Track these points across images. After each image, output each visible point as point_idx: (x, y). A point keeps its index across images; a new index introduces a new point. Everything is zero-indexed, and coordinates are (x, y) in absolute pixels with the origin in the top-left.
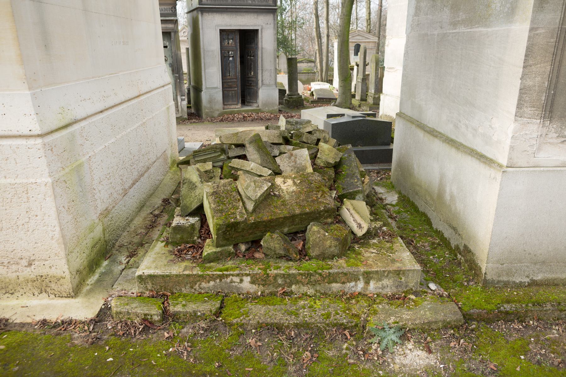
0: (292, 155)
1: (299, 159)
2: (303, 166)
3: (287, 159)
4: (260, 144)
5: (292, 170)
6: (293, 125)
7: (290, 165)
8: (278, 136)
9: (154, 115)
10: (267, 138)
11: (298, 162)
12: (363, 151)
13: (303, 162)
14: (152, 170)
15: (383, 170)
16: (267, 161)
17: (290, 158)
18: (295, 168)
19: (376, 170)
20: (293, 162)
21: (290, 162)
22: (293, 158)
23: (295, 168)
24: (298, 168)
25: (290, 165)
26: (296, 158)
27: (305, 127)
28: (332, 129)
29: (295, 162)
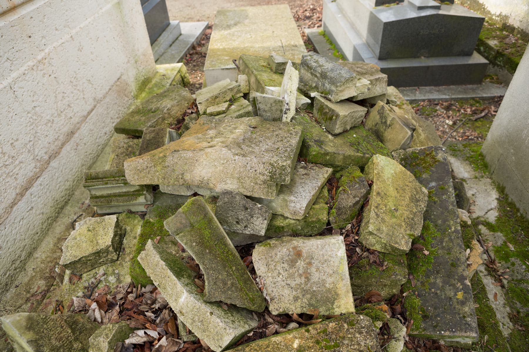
0: (299, 254)
1: (318, 270)
2: (329, 291)
3: (285, 265)
4: (207, 233)
5: (296, 299)
6: (316, 76)
7: (293, 284)
8: (265, 182)
9: (74, 32)
10: (235, 181)
11: (315, 277)
12: (428, 67)
13: (329, 280)
14: (85, 129)
15: (456, 100)
16: (225, 284)
17: (292, 263)
18: (305, 292)
19: (446, 100)
20: (300, 276)
21: (291, 276)
22: (301, 264)
23: (305, 292)
24: (314, 294)
25: (293, 284)
26: (310, 264)
27: (341, 91)
28: (384, 31)
29: (307, 277)
